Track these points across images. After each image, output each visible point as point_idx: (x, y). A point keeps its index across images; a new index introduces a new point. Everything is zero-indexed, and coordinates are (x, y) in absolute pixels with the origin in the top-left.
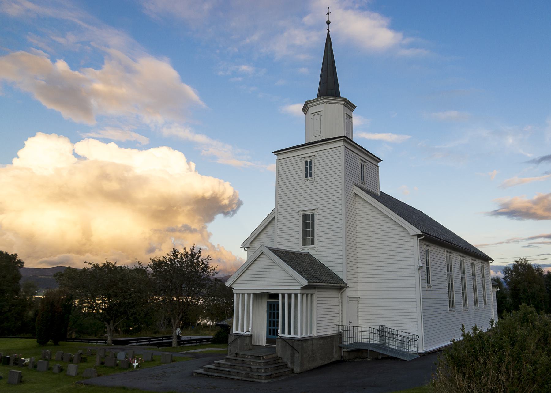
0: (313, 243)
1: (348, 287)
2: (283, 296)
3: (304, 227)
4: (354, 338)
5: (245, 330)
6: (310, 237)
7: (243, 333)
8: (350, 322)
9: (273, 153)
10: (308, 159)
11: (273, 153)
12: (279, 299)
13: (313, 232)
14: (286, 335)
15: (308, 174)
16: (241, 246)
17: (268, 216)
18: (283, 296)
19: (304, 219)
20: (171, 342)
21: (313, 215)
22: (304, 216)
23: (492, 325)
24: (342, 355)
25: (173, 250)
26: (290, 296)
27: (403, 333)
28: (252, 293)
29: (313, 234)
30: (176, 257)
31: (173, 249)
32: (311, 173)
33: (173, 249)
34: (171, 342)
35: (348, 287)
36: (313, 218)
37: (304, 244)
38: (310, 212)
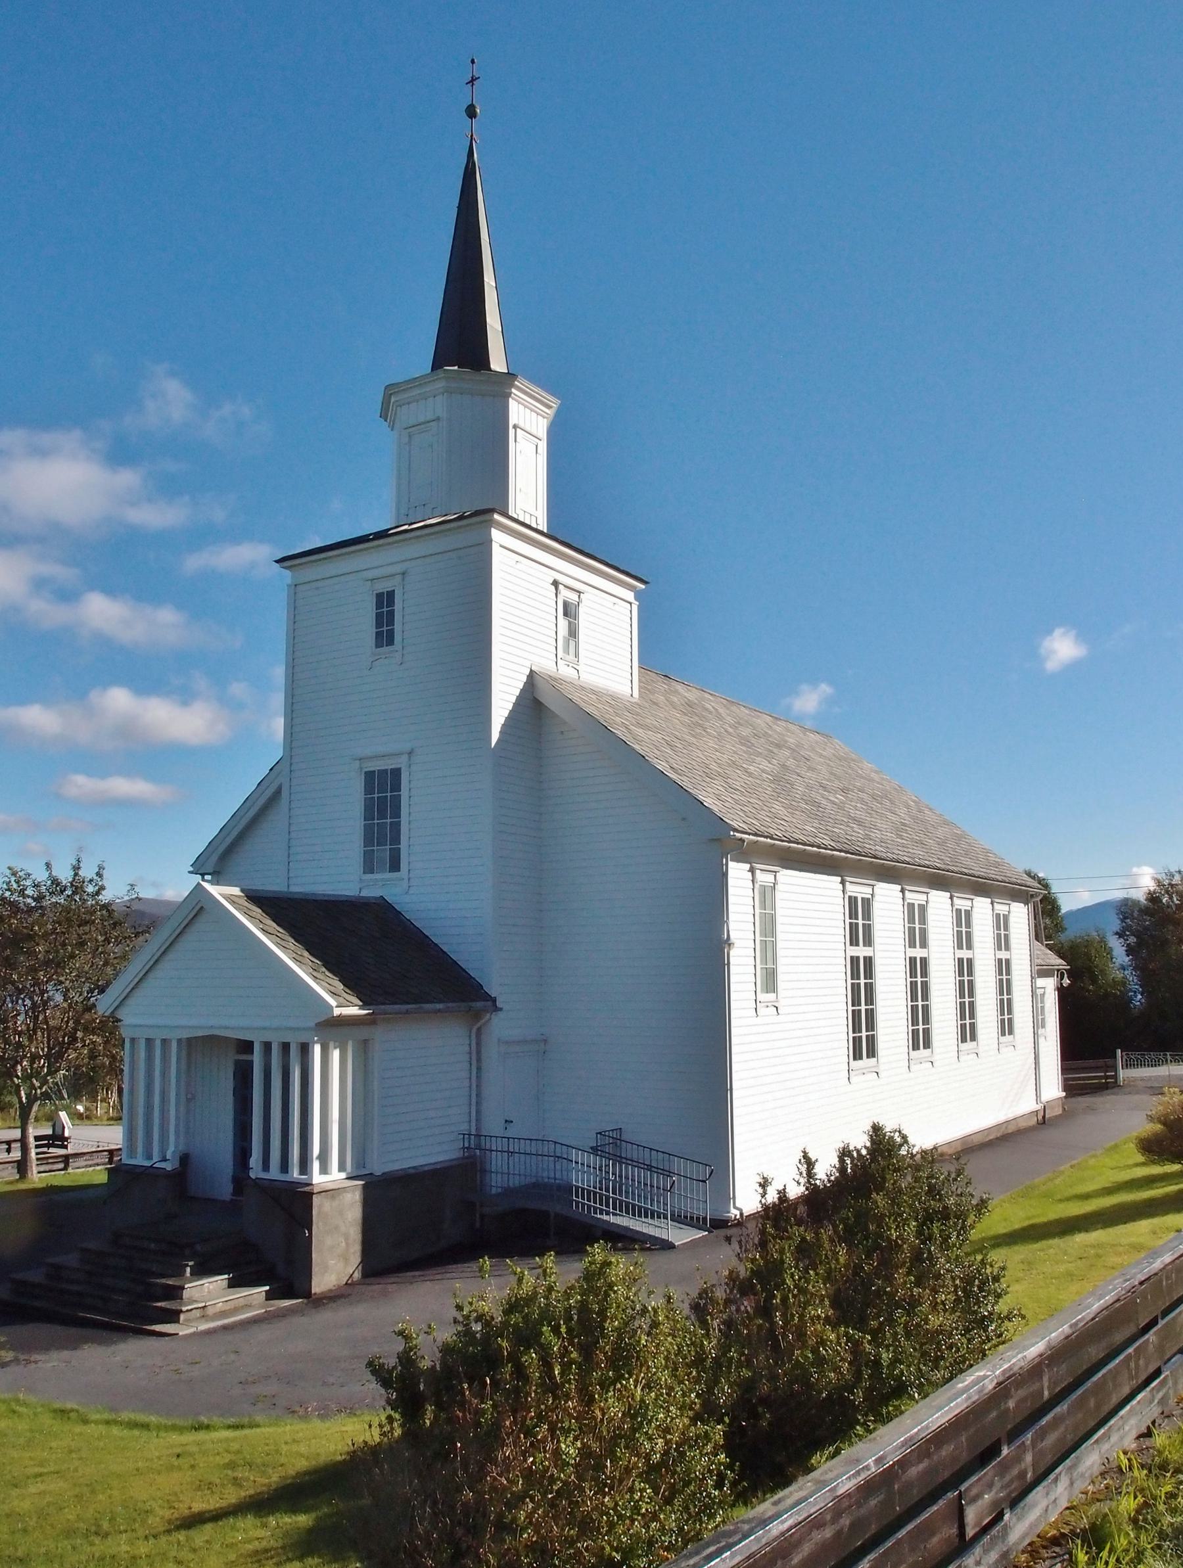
0: (395, 866)
1: (501, 1009)
2: (267, 1046)
3: (368, 815)
4: (509, 1174)
5: (155, 1159)
6: (388, 847)
7: (147, 1163)
8: (506, 1121)
9: (277, 562)
10: (383, 587)
11: (277, 562)
12: (253, 1053)
13: (396, 828)
14: (274, 1173)
15: (385, 636)
16: (191, 869)
17: (271, 770)
18: (267, 1046)
19: (369, 789)
20: (965, 910)
21: (397, 773)
22: (369, 776)
23: (764, 1195)
24: (478, 1225)
25: (9, 871)
26: (286, 1047)
27: (654, 1153)
28: (174, 1035)
29: (396, 839)
30: (22, 892)
31: (10, 868)
32: (394, 633)
33: (10, 868)
34: (965, 910)
35: (501, 1009)
36: (397, 786)
37: (369, 868)
38: (388, 765)
